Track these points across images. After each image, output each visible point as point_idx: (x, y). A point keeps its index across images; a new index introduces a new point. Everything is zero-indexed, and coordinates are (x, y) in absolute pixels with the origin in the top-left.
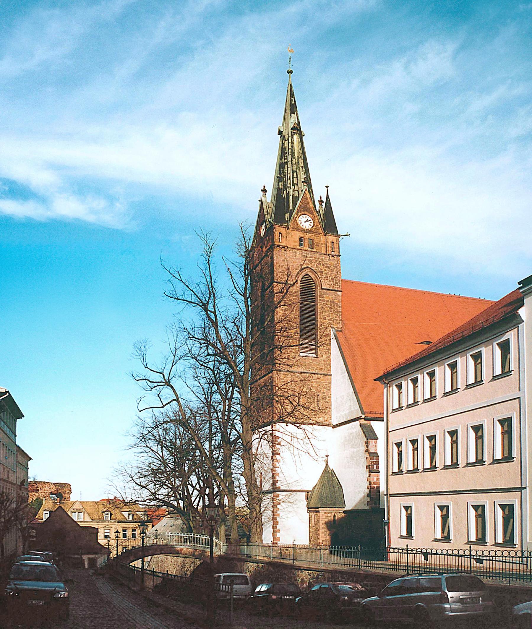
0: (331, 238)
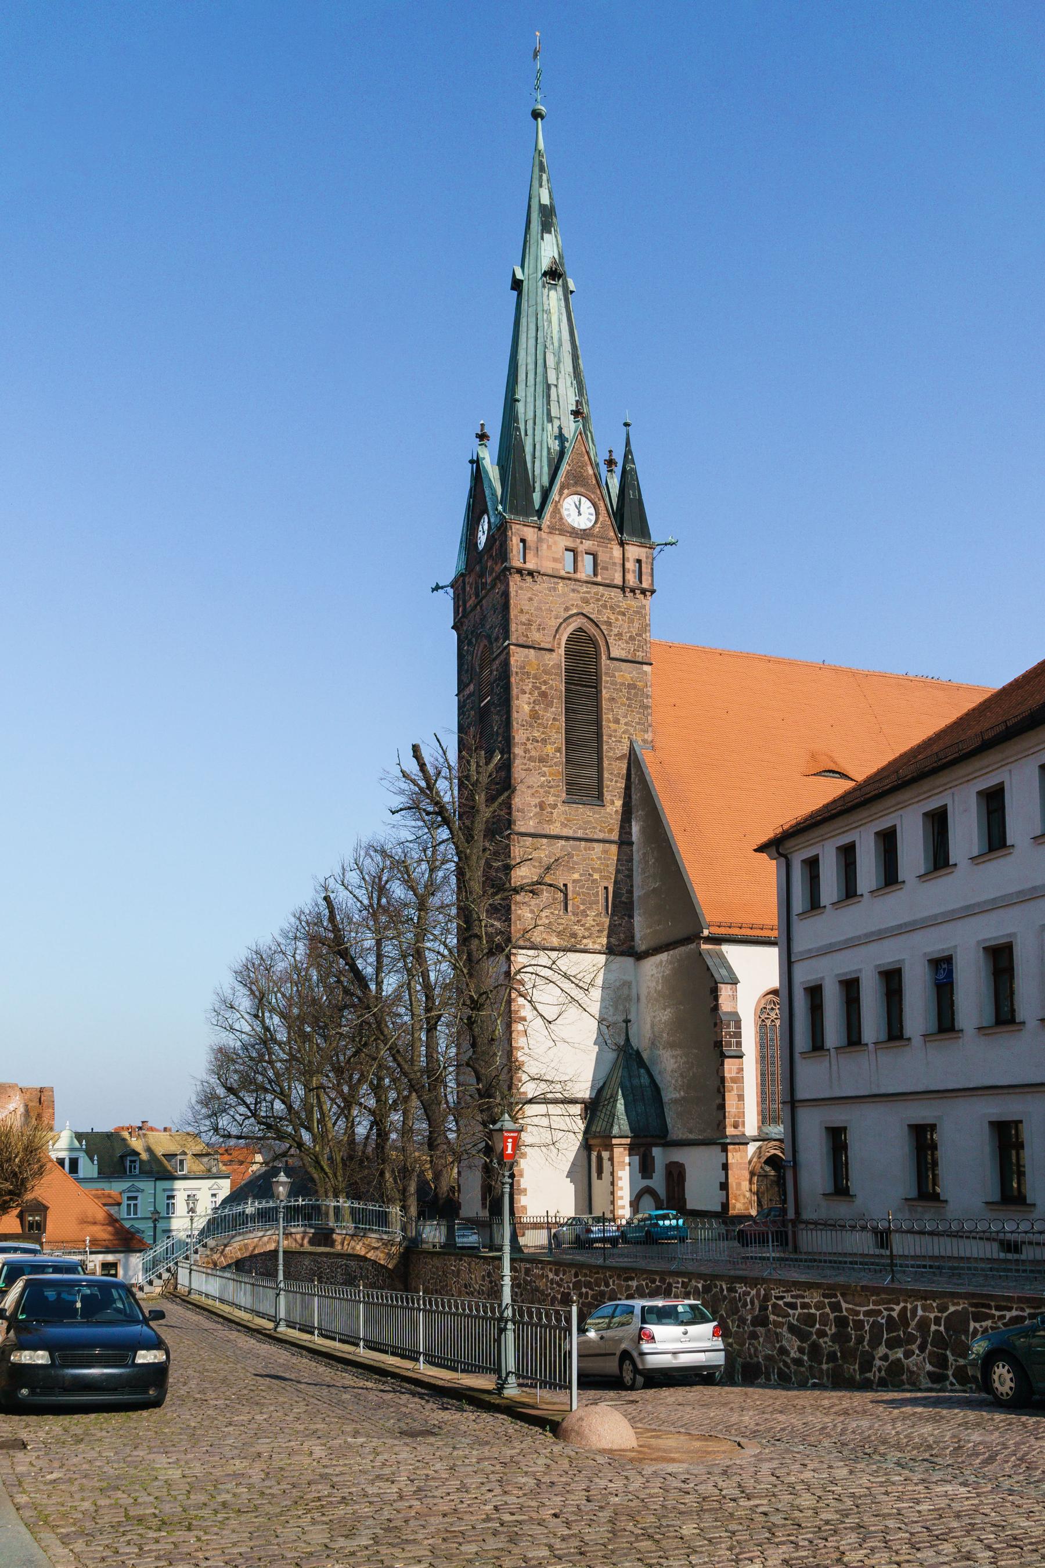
0: (634, 552)
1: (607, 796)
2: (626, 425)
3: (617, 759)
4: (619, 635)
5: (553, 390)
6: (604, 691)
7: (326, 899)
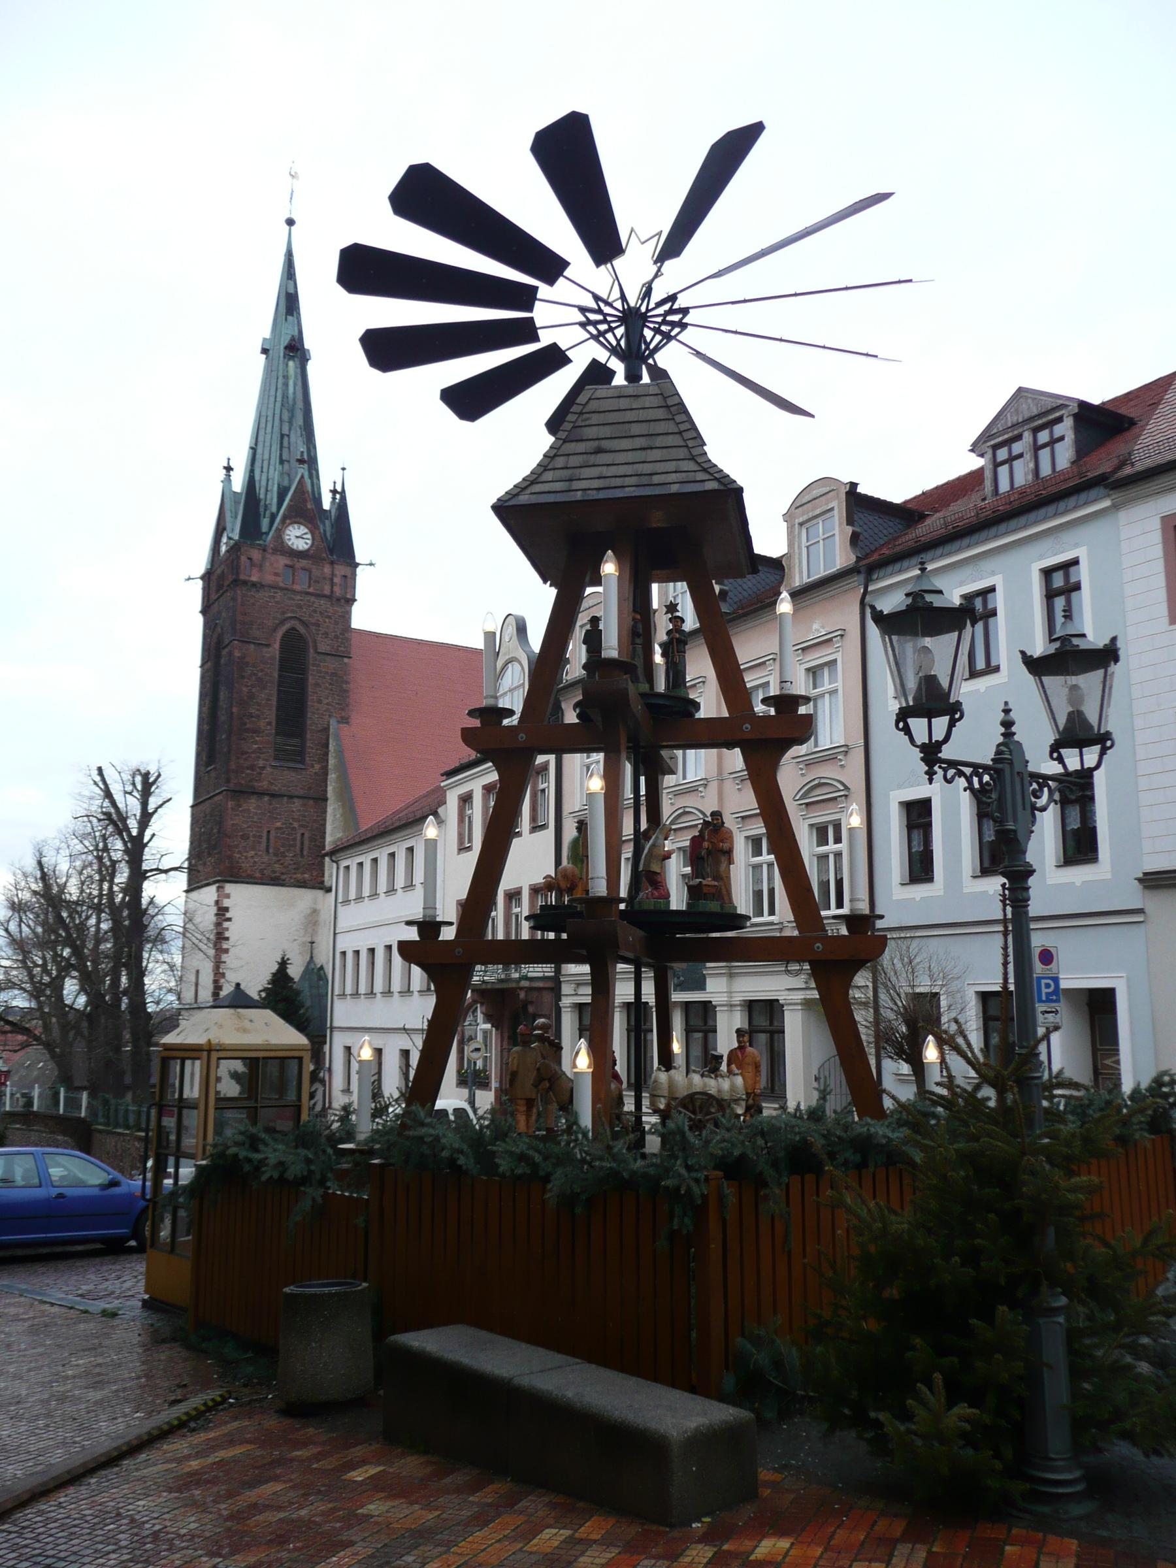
2: (344, 469)
5: (286, 438)
6: (310, 678)
7: (40, 863)
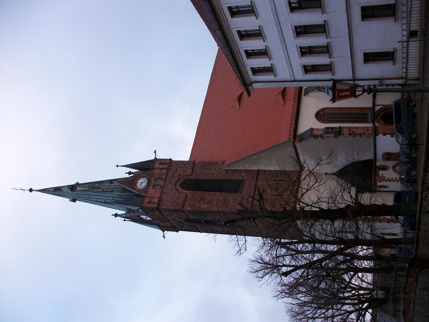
1: (240, 178)
3: (227, 174)
4: (184, 171)
